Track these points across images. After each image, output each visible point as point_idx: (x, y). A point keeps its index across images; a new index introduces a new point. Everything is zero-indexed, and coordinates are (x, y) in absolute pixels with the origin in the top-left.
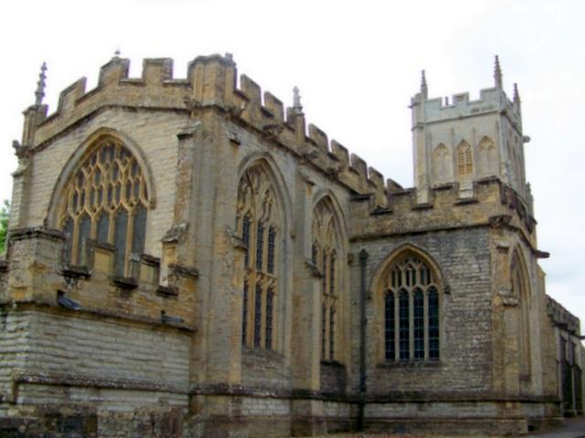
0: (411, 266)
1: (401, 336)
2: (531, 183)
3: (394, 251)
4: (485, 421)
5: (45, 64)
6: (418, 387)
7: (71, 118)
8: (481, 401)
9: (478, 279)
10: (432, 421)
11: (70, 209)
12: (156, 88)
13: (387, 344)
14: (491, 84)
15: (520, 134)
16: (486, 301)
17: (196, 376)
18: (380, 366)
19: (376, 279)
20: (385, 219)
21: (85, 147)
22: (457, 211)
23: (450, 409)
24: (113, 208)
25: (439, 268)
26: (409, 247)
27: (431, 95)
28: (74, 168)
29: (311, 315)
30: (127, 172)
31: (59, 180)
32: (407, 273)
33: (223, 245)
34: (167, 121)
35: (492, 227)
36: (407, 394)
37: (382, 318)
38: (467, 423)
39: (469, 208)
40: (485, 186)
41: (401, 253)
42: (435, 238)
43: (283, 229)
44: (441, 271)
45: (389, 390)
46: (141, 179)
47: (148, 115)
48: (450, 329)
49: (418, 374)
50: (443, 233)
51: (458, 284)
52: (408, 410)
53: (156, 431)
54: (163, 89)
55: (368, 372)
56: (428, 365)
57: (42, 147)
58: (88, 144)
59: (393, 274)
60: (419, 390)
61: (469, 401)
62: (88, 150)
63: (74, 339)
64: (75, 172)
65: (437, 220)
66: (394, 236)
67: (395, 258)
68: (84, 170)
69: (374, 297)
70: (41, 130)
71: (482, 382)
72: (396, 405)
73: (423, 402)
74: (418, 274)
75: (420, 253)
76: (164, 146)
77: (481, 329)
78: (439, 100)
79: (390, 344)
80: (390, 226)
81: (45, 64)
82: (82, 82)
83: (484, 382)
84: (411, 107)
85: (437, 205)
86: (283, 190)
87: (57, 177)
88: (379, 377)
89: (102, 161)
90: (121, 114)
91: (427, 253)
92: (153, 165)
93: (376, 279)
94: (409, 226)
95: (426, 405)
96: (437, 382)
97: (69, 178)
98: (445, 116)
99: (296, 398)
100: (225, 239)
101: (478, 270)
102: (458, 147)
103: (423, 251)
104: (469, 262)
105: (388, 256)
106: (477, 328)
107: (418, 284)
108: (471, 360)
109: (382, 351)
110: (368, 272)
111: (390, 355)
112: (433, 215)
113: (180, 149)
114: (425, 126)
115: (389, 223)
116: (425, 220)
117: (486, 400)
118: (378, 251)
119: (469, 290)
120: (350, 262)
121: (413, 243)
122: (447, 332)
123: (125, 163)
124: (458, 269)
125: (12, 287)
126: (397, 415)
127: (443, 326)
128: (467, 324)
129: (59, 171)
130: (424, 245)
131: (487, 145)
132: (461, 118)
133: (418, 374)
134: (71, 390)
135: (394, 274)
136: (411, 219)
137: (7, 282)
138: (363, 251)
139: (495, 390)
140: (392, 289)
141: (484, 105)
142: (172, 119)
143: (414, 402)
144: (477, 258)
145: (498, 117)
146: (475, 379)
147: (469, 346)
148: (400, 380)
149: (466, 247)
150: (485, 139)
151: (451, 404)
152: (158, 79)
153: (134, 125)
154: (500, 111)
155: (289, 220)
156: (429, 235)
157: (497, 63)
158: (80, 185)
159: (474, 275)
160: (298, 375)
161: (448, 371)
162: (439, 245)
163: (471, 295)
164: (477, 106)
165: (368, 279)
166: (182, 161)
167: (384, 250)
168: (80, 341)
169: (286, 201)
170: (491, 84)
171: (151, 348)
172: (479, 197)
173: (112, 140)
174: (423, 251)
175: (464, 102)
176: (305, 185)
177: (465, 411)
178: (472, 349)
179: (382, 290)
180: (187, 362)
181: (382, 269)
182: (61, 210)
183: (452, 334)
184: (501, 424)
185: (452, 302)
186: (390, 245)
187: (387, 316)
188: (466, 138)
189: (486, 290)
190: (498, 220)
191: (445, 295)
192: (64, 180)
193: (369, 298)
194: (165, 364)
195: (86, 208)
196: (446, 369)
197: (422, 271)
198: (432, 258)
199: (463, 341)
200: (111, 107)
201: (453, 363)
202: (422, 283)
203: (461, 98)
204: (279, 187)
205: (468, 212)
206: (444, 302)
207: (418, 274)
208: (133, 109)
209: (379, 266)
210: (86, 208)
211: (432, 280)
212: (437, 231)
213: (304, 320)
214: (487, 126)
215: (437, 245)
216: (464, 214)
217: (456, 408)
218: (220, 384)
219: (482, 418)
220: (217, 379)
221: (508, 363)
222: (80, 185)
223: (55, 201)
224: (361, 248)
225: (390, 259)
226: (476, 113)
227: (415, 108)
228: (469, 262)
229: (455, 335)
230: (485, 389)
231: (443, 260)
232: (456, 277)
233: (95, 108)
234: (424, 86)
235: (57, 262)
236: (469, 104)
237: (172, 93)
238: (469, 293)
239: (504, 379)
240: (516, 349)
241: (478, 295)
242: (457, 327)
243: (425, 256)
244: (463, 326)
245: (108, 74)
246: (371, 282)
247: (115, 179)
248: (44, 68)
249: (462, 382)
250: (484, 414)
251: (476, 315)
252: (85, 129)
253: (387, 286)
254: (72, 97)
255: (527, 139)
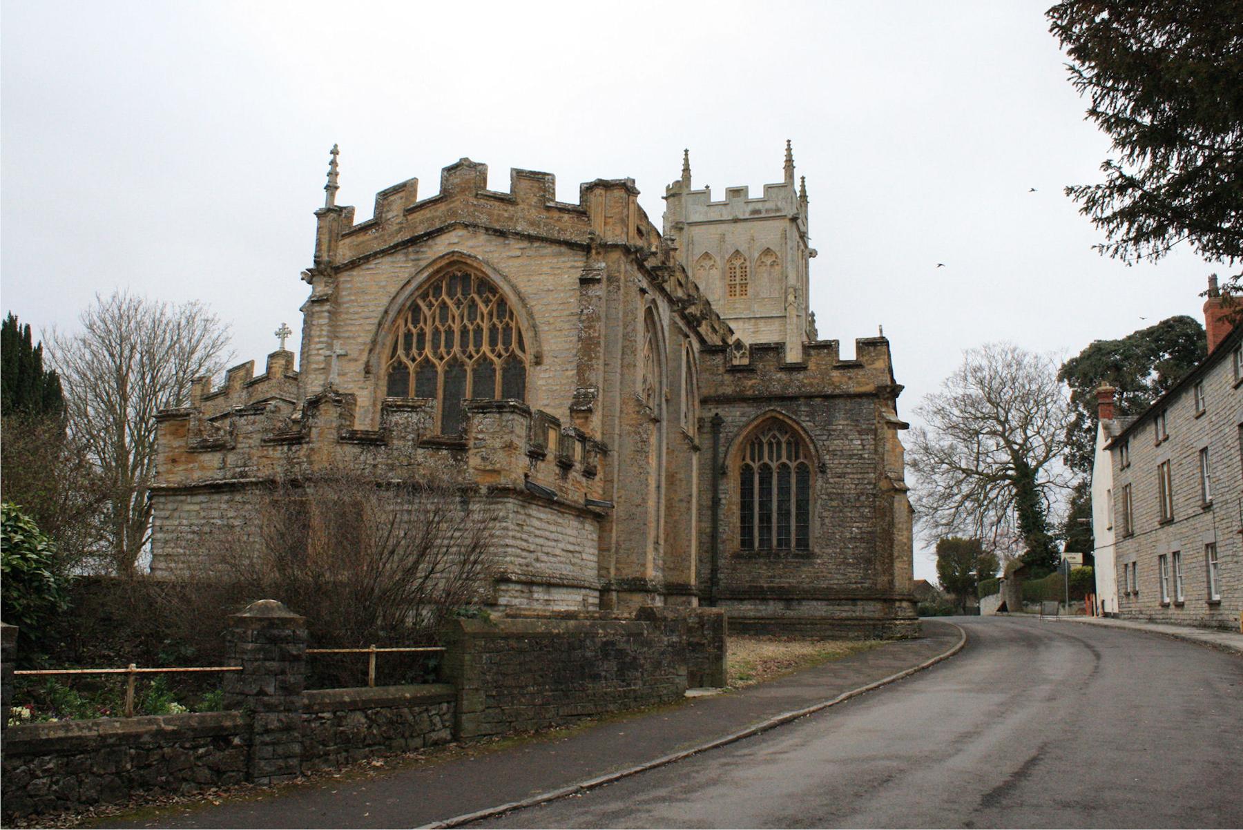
0: (774, 437)
1: (761, 520)
2: (956, 364)
3: (757, 417)
4: (867, 622)
5: (336, 146)
6: (785, 582)
7: (400, 230)
8: (862, 599)
9: (861, 457)
10: (803, 622)
11: (401, 352)
12: (533, 211)
13: (743, 528)
14: (780, 178)
15: (806, 247)
16: (869, 483)
17: (608, 569)
18: (736, 556)
19: (733, 450)
20: (745, 377)
21: (425, 274)
22: (835, 373)
23: (825, 608)
24: (471, 357)
25: (812, 441)
26: (774, 414)
27: (696, 185)
28: (407, 299)
29: (691, 496)
30: (491, 314)
31: (386, 312)
32: (770, 444)
33: (634, 416)
34: (554, 255)
35: (878, 398)
36: (772, 589)
37: (736, 498)
38: (846, 625)
39: (852, 373)
40: (871, 348)
41: (763, 421)
42: (807, 405)
43: (657, 390)
44: (815, 447)
45: (747, 585)
46: (513, 324)
47: (525, 244)
48: (825, 514)
49: (785, 567)
50: (818, 400)
51: (836, 462)
52: (773, 608)
53: (706, 632)
54: (545, 214)
55: (722, 562)
56: (796, 556)
57: (353, 265)
58: (431, 270)
59: (753, 444)
60: (787, 585)
61: (847, 599)
62: (429, 278)
63: (532, 529)
64: (408, 304)
65: (811, 385)
66: (756, 400)
67: (756, 427)
68: (420, 302)
69: (730, 474)
70: (347, 241)
71: (862, 578)
72: (758, 602)
73: (792, 599)
74: (784, 446)
75: (790, 422)
76: (551, 288)
77: (862, 516)
78: (706, 192)
79: (746, 530)
80: (752, 387)
81: (336, 146)
82: (408, 188)
83: (865, 577)
84: (666, 198)
85: (812, 365)
86: (661, 344)
87: (382, 309)
88: (734, 569)
89: (451, 294)
90: (482, 237)
91: (798, 424)
92: (535, 309)
93: (733, 450)
94: (776, 388)
95: (795, 603)
96: (807, 577)
97: (399, 312)
98: (714, 215)
99: (672, 594)
100: (637, 409)
101: (860, 447)
102: (730, 260)
103: (795, 421)
104: (850, 437)
105: (748, 424)
106: (857, 515)
107: (784, 460)
108: (850, 552)
109: (738, 538)
110: (722, 441)
111: (747, 542)
112: (806, 378)
113: (582, 295)
114: (686, 227)
115: (750, 383)
116: (797, 384)
117: (868, 599)
118: (734, 416)
119: (849, 471)
120: (700, 428)
121: (781, 411)
122: (822, 518)
123: (487, 302)
124: (837, 444)
125: (475, 468)
126: (759, 615)
127: (816, 509)
128: (846, 510)
129: (385, 301)
130: (795, 413)
131: (769, 260)
132: (736, 221)
133: (785, 567)
134: (535, 588)
135: (754, 443)
136: (780, 380)
137: (466, 463)
138: (717, 414)
139: (879, 587)
140: (751, 463)
141: (769, 205)
142: (561, 254)
143: (780, 599)
144: (860, 433)
145: (786, 224)
146: (854, 574)
147: (848, 535)
148: (762, 574)
149: (846, 419)
150: (768, 251)
151: (826, 602)
152: (535, 199)
153: (504, 255)
154: (790, 217)
155: (665, 380)
156: (802, 401)
157: (789, 149)
158: (415, 322)
159: (855, 452)
160: (672, 566)
161: (823, 564)
162: (813, 414)
163: (851, 476)
164: (759, 206)
165: (722, 449)
166: (585, 311)
167: (743, 415)
168: (538, 532)
169: (663, 358)
170: (780, 178)
171: (576, 537)
172: (864, 360)
173: (466, 268)
174: (795, 421)
175: (742, 199)
176: (681, 337)
177: (843, 611)
178: (851, 538)
179: (739, 463)
180: (596, 552)
181: (741, 438)
182: (387, 351)
183: (827, 521)
184: (896, 625)
185: (827, 482)
186: (751, 411)
187: (743, 495)
188: (741, 250)
189: (870, 470)
190: (888, 390)
191: (820, 475)
192: (392, 314)
193: (724, 473)
194: (585, 556)
195: (428, 351)
196: (819, 561)
197: (789, 443)
198: (804, 430)
199: (841, 529)
200: (466, 226)
201: (829, 554)
202: (789, 458)
203: (736, 193)
204: (657, 341)
205: (850, 378)
206: (818, 483)
207: (784, 446)
208: (501, 234)
209: (737, 435)
210: (428, 351)
211: (801, 455)
212: (810, 397)
213: (681, 500)
214: (769, 234)
215: (811, 415)
216: (846, 379)
217: (831, 607)
218: (634, 579)
219: (862, 619)
220: (630, 573)
221: (897, 557)
222: (415, 322)
223: (379, 339)
224: (714, 411)
225: (750, 427)
226: (757, 215)
227: (671, 199)
228: (850, 437)
229: (831, 522)
230: (866, 585)
231: (818, 433)
232: (833, 454)
233: (438, 225)
234: (686, 170)
235: (524, 441)
236: (748, 202)
237: (559, 220)
238: (849, 473)
239: (892, 575)
240: (905, 540)
241: (859, 476)
242: (834, 512)
243: (796, 427)
244: (841, 511)
245: (456, 180)
246: (726, 452)
247: (471, 320)
248: (335, 152)
249: (839, 577)
250: (866, 615)
251: (858, 499)
252: (424, 249)
253: (744, 460)
254: (397, 204)
255: (813, 254)
